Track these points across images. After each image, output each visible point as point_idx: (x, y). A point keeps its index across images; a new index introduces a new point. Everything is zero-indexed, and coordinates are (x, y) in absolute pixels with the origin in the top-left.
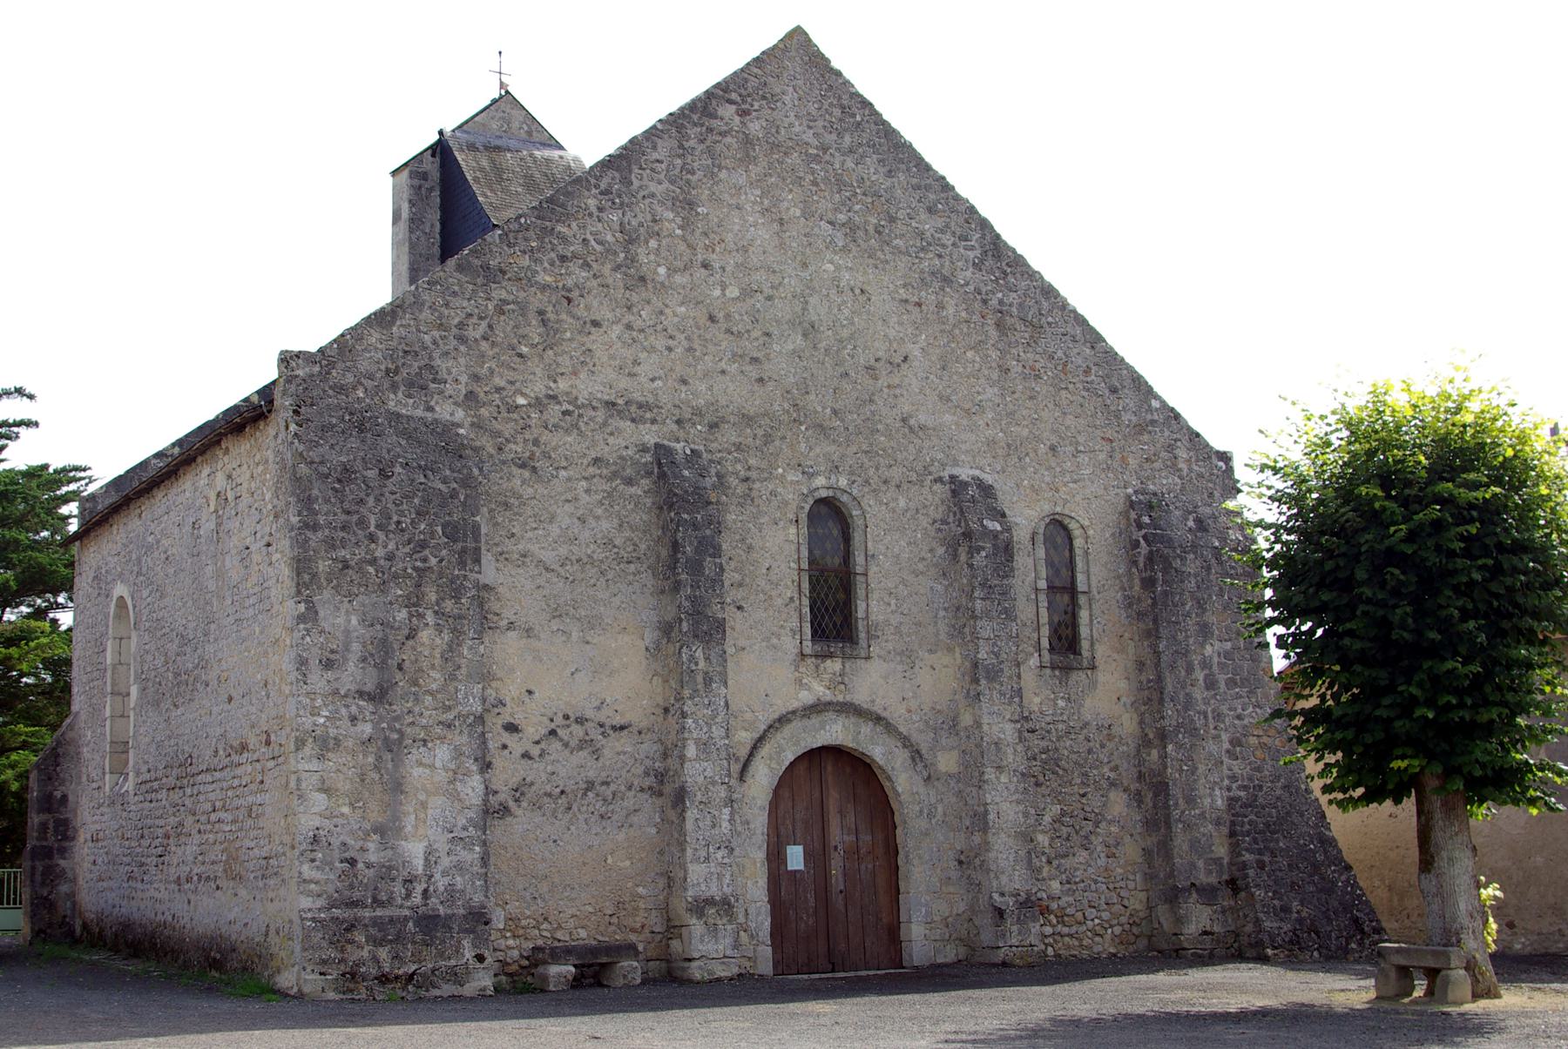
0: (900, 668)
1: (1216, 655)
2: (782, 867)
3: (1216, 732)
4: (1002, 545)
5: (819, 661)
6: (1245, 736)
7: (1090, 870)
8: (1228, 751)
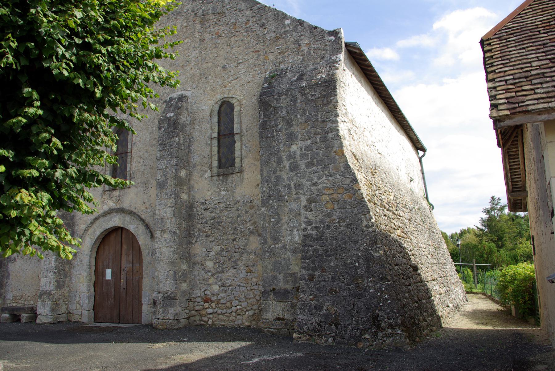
0: (142, 189)
1: (299, 150)
2: (104, 278)
3: (297, 196)
4: (172, 123)
5: (110, 193)
6: (319, 195)
7: (236, 280)
8: (305, 207)
